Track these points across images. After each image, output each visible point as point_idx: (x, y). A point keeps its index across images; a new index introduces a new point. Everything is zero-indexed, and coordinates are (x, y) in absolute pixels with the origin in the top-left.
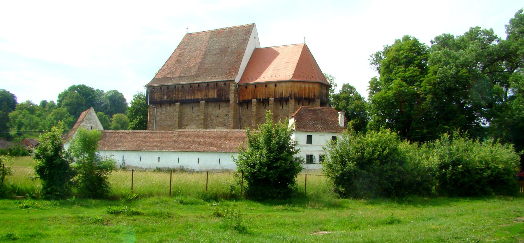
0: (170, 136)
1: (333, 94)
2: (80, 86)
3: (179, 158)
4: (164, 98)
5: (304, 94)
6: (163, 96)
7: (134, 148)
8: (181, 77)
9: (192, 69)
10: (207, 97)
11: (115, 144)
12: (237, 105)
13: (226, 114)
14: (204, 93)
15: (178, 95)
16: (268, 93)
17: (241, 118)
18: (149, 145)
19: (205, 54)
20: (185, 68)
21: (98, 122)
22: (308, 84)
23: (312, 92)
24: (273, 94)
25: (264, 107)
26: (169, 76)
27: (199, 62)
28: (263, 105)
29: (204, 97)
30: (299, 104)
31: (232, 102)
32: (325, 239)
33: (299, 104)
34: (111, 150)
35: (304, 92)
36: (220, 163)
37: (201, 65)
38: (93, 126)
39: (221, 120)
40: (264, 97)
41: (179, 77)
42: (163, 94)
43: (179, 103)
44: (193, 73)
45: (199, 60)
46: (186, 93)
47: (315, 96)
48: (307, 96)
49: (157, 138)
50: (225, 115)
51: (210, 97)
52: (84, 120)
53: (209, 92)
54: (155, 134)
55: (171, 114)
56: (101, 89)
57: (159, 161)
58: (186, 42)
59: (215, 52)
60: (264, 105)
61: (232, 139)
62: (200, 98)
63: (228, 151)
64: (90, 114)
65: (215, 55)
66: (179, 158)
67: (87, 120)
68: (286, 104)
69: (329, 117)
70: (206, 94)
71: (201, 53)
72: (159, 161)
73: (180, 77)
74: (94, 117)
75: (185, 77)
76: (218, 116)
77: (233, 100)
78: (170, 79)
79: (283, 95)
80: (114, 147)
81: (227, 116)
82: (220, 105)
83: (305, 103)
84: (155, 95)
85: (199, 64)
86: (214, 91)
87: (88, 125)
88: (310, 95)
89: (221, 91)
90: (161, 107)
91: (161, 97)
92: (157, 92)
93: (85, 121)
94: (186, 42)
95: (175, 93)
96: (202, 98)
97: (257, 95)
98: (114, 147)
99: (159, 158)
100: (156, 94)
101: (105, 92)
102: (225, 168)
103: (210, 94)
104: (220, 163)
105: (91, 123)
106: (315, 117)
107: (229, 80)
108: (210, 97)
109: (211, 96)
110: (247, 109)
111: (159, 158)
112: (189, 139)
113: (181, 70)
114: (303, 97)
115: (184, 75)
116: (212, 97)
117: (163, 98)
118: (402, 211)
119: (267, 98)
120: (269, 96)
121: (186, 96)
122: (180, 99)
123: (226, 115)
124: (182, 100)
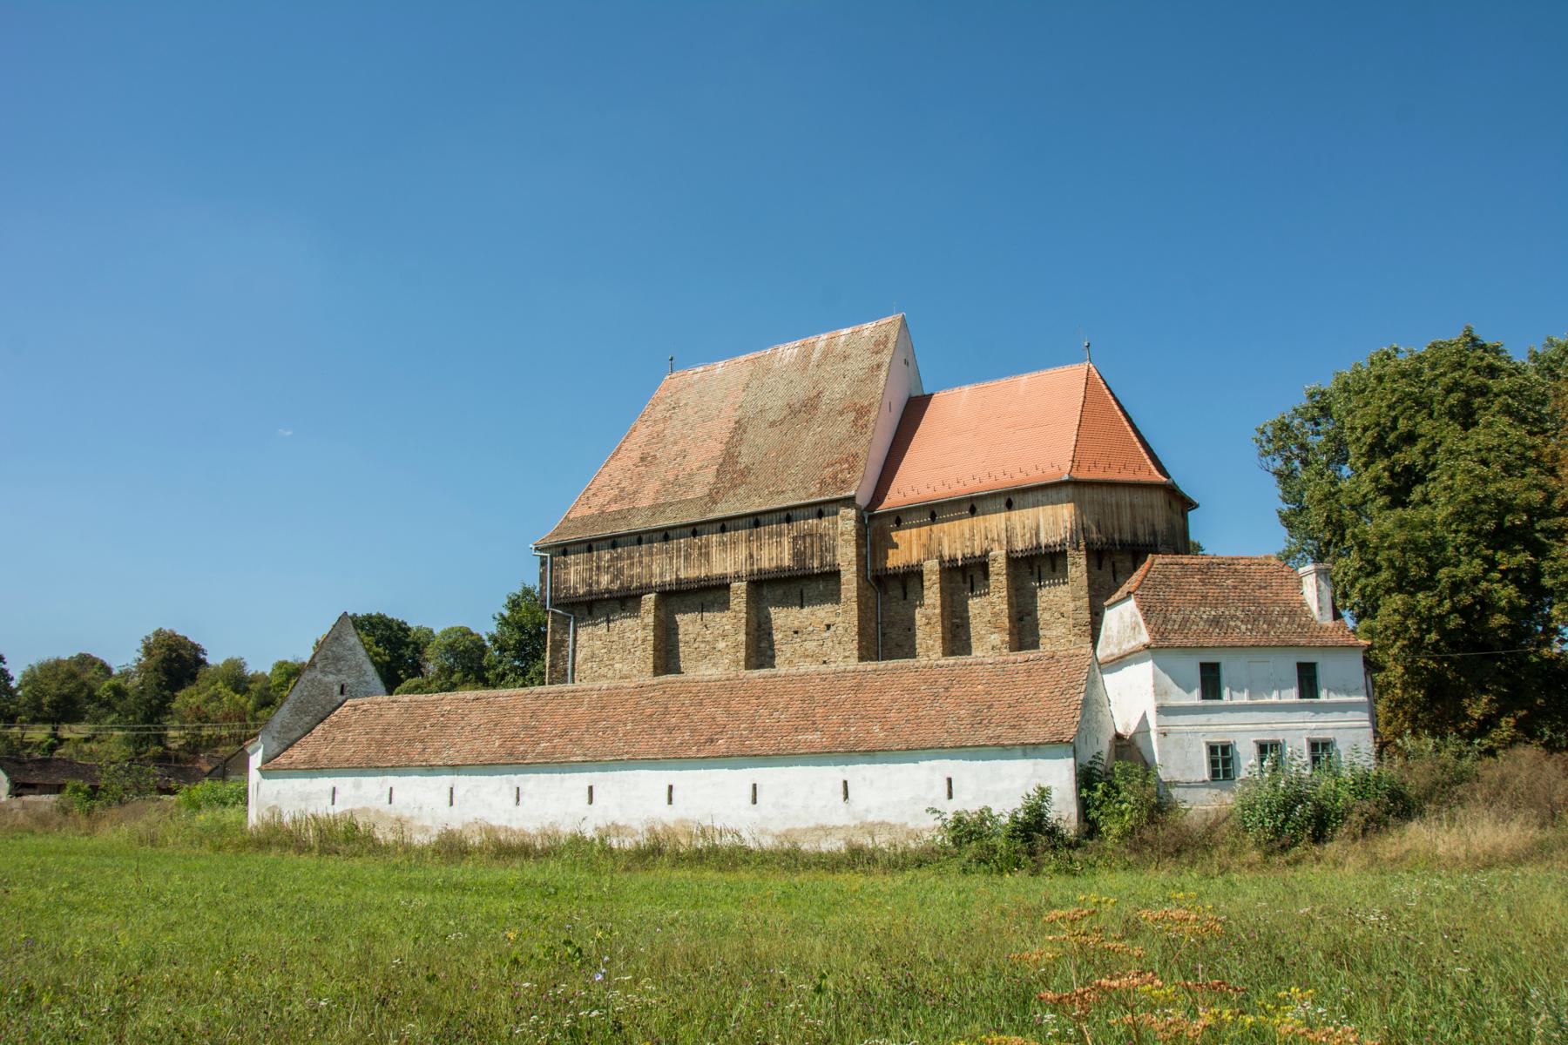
0: (632, 702)
1: (1398, 432)
2: (370, 617)
3: (671, 788)
4: (602, 579)
5: (1116, 527)
6: (598, 575)
7: (495, 753)
8: (660, 505)
9: (697, 478)
10: (755, 567)
11: (422, 741)
12: (866, 584)
13: (826, 622)
14: (742, 553)
15: (650, 567)
16: (983, 533)
17: (883, 635)
18: (549, 741)
19: (740, 426)
20: (671, 478)
21: (364, 667)
22: (1127, 490)
23: (1143, 522)
24: (1003, 535)
25: (969, 585)
26: (614, 507)
27: (719, 453)
28: (965, 582)
29: (744, 570)
30: (1100, 568)
31: (850, 576)
32: (1025, 1013)
33: (1100, 568)
34: (406, 766)
35: (1116, 523)
36: (846, 796)
37: (729, 459)
38: (349, 681)
39: (811, 646)
40: (968, 551)
41: (650, 507)
42: (598, 568)
43: (653, 596)
44: (699, 491)
45: (717, 449)
46: (678, 557)
47: (1154, 533)
48: (1127, 537)
49: (580, 711)
50: (823, 627)
51: (767, 566)
52: (316, 660)
53: (760, 548)
54: (574, 697)
55: (628, 634)
56: (426, 625)
57: (591, 802)
58: (669, 401)
59: (771, 417)
60: (969, 580)
61: (887, 696)
62: (730, 570)
63: (880, 745)
64: (337, 639)
65: (772, 424)
66: (671, 788)
67: (325, 662)
68: (1054, 570)
69: (1265, 588)
70: (751, 556)
71: (721, 428)
72: (591, 802)
73: (656, 508)
74: (350, 650)
75: (671, 504)
76: (796, 632)
77: (855, 568)
78: (623, 515)
79: (1042, 535)
80: (419, 754)
81: (833, 628)
82: (805, 591)
83: (1121, 561)
84: (569, 574)
85: (721, 460)
86: (779, 543)
87: (331, 678)
88: (1140, 532)
89: (808, 540)
90: (590, 613)
91: (591, 578)
92: (577, 564)
93: (318, 666)
94: (669, 401)
95: (641, 562)
96: (737, 573)
97: (940, 544)
98: (419, 754)
99: (591, 788)
100: (572, 569)
101: (437, 631)
102: (872, 818)
103: (765, 552)
104: (846, 796)
105: (340, 671)
106: (1213, 592)
107: (835, 496)
108: (765, 564)
109: (771, 560)
110: (905, 598)
111: (591, 788)
112: (710, 710)
113: (658, 483)
114: (1113, 540)
115: (669, 499)
116: (774, 564)
117: (598, 583)
118: (717, 876)
119: (978, 553)
120: (985, 545)
121: (678, 570)
122: (656, 581)
123: (828, 627)
124: (664, 584)
